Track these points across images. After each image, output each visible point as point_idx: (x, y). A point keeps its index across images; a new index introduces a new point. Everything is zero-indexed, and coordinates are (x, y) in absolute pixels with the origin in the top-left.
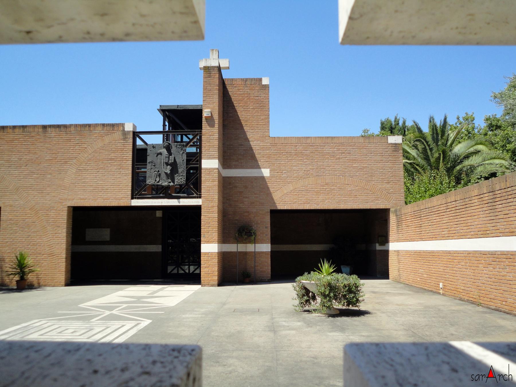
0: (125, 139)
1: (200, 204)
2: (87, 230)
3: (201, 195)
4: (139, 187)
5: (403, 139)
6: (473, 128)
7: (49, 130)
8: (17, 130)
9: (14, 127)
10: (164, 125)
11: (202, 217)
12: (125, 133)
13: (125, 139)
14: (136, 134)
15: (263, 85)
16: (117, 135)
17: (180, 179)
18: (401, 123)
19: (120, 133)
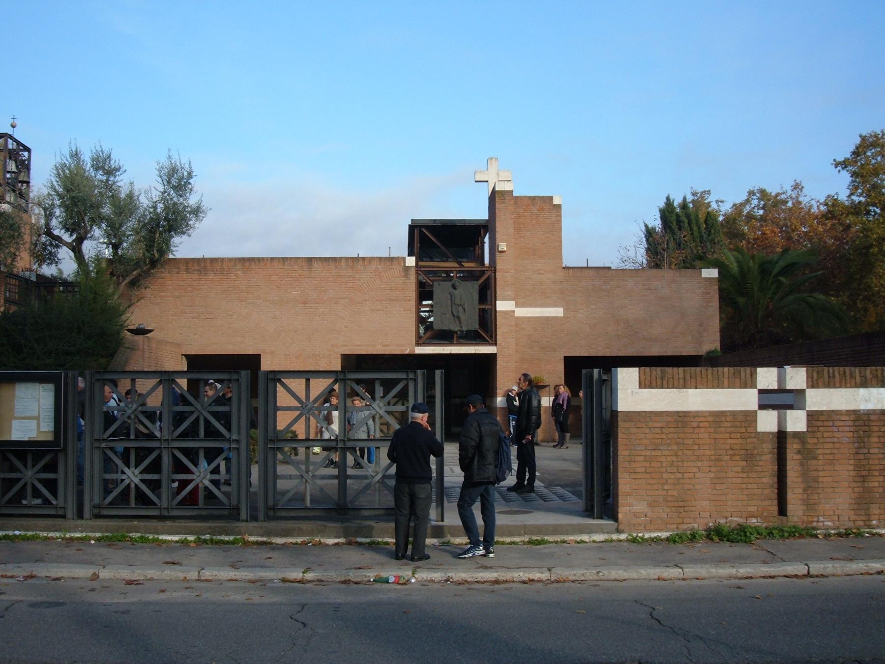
1: (495, 352)
7: (315, 264)
8: (275, 263)
9: (272, 259)
15: (555, 205)
16: (397, 269)
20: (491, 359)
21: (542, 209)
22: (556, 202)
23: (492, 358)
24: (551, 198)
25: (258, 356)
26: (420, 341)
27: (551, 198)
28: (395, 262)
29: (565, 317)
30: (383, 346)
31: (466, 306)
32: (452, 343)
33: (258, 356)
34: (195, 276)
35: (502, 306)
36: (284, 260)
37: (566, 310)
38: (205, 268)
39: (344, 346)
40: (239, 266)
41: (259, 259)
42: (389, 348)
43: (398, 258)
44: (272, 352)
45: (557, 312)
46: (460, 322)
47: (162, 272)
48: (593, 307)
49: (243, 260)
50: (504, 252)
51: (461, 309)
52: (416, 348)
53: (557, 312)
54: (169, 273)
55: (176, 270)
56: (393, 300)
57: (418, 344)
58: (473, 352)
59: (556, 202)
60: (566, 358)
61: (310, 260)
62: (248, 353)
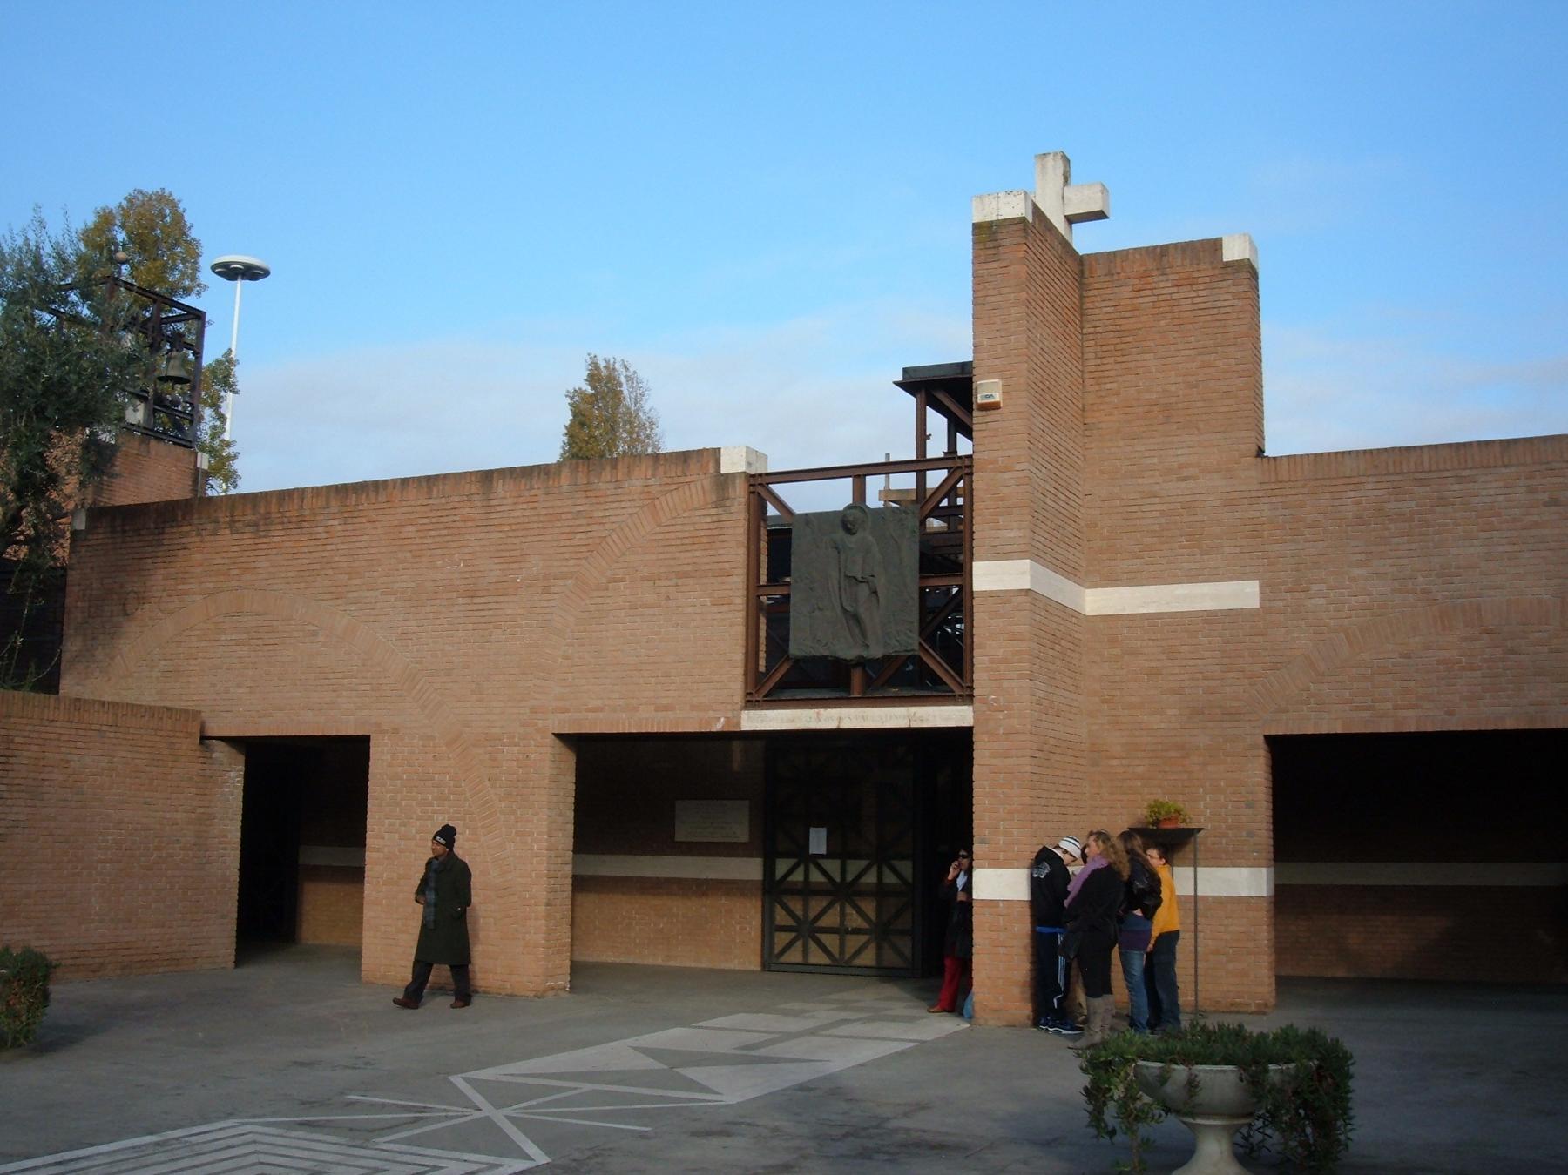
0: (721, 502)
1: (968, 722)
2: (679, 804)
3: (972, 688)
4: (783, 672)
5: (769, 929)
6: (20, 263)
7: (500, 487)
8: (412, 493)
9: (405, 481)
10: (922, 437)
11: (977, 771)
12: (724, 481)
13: (721, 502)
14: (759, 486)
15: (1229, 265)
16: (699, 487)
17: (905, 637)
18: (231, 451)
19: (707, 483)
20: (955, 747)
21: (1188, 281)
22: (1231, 253)
23: (961, 740)
24: (1215, 245)
25: (364, 741)
26: (762, 691)
27: (1215, 245)
28: (693, 466)
29: (1265, 610)
30: (693, 708)
31: (881, 582)
32: (846, 700)
33: (364, 741)
34: (247, 539)
35: (990, 576)
36: (430, 481)
37: (1269, 590)
38: (267, 516)
39: (565, 710)
40: (335, 506)
41: (376, 484)
42: (671, 715)
43: (700, 452)
44: (396, 731)
45: (1243, 594)
46: (863, 634)
47: (186, 535)
48: (1357, 572)
49: (342, 491)
50: (995, 406)
51: (864, 591)
52: (745, 714)
53: (1243, 594)
54: (199, 535)
55: (210, 527)
56: (686, 575)
57: (750, 703)
58: (903, 724)
59: (1231, 253)
60: (1271, 741)
61: (487, 477)
62: (327, 733)
